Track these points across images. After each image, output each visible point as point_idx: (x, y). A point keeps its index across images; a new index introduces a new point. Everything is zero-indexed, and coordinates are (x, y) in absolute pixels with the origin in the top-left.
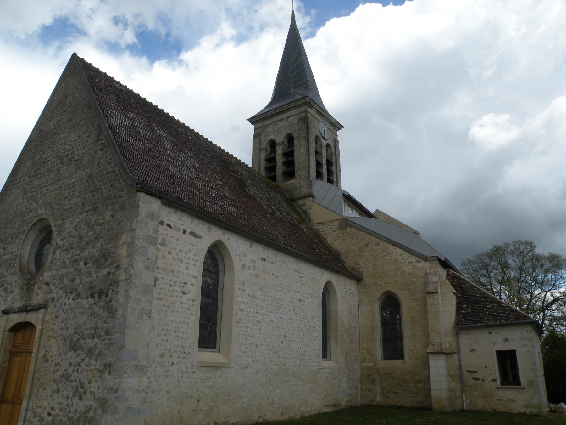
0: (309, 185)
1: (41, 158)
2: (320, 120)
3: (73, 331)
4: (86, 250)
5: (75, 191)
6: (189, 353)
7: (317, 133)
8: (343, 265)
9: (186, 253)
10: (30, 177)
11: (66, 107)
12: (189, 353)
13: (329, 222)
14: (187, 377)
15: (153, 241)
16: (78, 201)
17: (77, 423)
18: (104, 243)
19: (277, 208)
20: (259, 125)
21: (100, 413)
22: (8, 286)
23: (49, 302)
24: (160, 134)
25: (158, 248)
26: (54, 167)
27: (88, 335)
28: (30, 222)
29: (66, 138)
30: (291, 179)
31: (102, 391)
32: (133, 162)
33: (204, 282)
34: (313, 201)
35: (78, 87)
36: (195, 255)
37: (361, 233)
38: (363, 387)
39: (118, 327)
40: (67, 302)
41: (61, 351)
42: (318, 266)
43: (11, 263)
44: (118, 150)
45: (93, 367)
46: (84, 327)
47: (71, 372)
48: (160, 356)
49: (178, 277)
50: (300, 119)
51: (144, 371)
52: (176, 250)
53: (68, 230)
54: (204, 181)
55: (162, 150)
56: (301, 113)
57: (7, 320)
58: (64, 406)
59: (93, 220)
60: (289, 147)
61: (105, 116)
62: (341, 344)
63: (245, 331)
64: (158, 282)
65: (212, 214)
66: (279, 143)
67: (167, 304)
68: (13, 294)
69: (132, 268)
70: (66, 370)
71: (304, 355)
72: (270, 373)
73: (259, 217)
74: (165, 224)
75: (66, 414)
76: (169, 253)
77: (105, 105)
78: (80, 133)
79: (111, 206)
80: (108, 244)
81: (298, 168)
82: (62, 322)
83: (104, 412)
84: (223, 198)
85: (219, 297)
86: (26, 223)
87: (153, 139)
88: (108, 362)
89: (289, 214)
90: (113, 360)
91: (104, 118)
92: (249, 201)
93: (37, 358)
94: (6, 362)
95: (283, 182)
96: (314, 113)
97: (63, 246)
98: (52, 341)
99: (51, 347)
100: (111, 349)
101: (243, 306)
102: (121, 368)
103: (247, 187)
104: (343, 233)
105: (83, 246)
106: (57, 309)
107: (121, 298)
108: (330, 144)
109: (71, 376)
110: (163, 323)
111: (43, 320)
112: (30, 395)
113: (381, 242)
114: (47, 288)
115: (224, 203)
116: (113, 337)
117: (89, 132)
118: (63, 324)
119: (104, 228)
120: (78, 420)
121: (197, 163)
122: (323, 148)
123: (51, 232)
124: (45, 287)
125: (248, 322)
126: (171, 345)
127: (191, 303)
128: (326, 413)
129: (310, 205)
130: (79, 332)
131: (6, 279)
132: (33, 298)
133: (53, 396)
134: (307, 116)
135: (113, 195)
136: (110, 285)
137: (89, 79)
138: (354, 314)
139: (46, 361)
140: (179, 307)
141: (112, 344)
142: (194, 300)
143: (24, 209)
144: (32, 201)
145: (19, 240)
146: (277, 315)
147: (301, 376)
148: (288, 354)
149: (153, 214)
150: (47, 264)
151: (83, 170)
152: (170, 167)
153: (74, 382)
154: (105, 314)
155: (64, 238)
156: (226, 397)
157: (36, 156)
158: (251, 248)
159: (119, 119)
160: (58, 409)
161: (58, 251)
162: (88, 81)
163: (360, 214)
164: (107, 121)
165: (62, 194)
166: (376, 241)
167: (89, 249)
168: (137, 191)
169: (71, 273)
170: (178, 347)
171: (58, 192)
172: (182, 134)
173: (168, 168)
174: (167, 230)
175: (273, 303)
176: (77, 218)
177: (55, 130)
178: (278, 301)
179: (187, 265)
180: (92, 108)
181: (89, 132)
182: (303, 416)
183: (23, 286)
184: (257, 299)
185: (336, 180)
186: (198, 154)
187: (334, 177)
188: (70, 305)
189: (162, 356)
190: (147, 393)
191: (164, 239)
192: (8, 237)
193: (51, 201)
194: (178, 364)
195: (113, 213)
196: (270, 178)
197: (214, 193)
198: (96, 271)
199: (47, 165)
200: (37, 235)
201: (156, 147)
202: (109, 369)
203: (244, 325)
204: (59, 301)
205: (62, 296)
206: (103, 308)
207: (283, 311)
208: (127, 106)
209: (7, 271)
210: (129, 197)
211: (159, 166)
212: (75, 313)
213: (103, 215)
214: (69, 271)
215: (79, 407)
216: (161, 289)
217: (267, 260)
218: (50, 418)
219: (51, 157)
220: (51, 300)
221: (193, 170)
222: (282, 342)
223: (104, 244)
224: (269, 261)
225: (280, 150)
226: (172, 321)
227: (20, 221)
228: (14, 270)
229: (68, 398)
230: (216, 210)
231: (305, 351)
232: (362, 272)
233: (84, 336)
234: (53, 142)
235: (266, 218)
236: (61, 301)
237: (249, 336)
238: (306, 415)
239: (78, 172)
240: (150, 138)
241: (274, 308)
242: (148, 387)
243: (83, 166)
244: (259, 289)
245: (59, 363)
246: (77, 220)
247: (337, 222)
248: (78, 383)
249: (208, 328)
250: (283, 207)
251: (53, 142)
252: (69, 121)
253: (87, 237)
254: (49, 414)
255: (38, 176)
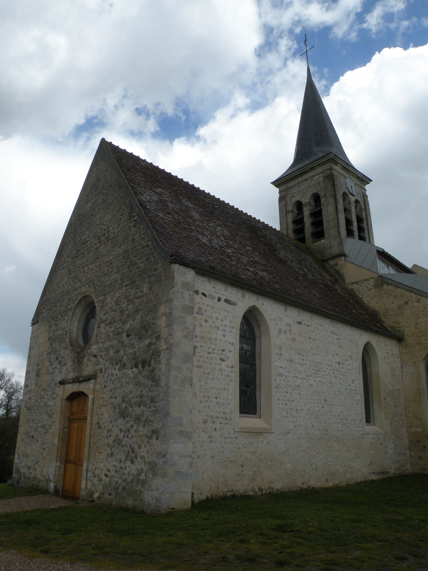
0: (340, 244)
1: (81, 239)
2: (346, 176)
3: (121, 399)
4: (127, 323)
5: (113, 267)
6: (230, 419)
7: (344, 190)
8: (383, 325)
9: (222, 320)
10: (72, 258)
11: (99, 190)
12: (230, 419)
13: (364, 281)
14: (230, 443)
15: (189, 310)
16: (117, 277)
17: (131, 484)
18: (144, 315)
19: (309, 270)
20: (284, 187)
21: (151, 476)
22: (61, 359)
23: (98, 373)
24: (187, 205)
25: (195, 317)
26: (93, 247)
27: (135, 403)
28: (76, 300)
29: (102, 219)
30: (320, 239)
31: (151, 456)
32: (165, 235)
33: (241, 349)
34: (345, 260)
35: (109, 169)
36: (231, 322)
37: (399, 290)
38: (413, 454)
39: (162, 395)
40: (114, 372)
41: (112, 418)
42: (356, 327)
43: (62, 338)
44: (150, 225)
45: (141, 433)
46: (131, 396)
47: (122, 437)
48: (203, 422)
49: (216, 345)
50: (325, 177)
51: (188, 436)
52: (212, 318)
53: (109, 305)
54: (234, 248)
55: (191, 221)
56: (326, 170)
57: (64, 390)
58: (118, 468)
59: (132, 294)
60: (316, 206)
61: (135, 194)
62: (385, 407)
63: (285, 396)
64: (197, 350)
65: (245, 280)
66: (306, 203)
67: (207, 372)
68: (67, 366)
69: (171, 338)
70: (117, 436)
71: (346, 419)
72: (312, 438)
73: (292, 281)
74: (200, 293)
75: (120, 476)
76: (206, 321)
77: (134, 183)
78: (114, 212)
79: (148, 280)
80: (147, 316)
81: (327, 228)
82: (111, 391)
83: (154, 475)
84: (254, 263)
85: (257, 362)
86: (72, 301)
87: (182, 211)
88: (155, 428)
89: (321, 275)
90: (159, 426)
91: (134, 196)
92: (280, 265)
93: (91, 425)
94: (66, 428)
95: (313, 243)
96: (340, 169)
97: (106, 320)
98: (103, 409)
99: (102, 414)
100: (157, 416)
101: (281, 371)
102: (167, 434)
103: (277, 251)
104: (380, 291)
105: (124, 319)
106: (106, 379)
107: (163, 367)
108: (359, 200)
109: (122, 441)
110: (205, 390)
111: (94, 390)
112: (89, 458)
113: (423, 299)
114: (95, 360)
115: (256, 268)
116: (158, 404)
117: (121, 211)
118: (112, 393)
119: (143, 301)
120: (132, 481)
121: (226, 231)
122: (352, 205)
123: (95, 307)
124: (92, 358)
125: (288, 387)
126: (213, 411)
127: (230, 369)
128: (373, 481)
129: (343, 264)
130: (126, 400)
131: (60, 353)
132: (84, 370)
133: (108, 459)
134: (332, 173)
135: (149, 269)
136: (152, 355)
137: (117, 161)
138: (397, 376)
139: (100, 427)
140: (218, 374)
141: (157, 411)
142: (232, 367)
143: (70, 288)
144: (76, 280)
145: (68, 316)
146: (316, 379)
147: (344, 442)
148: (330, 419)
149: (188, 284)
150: (94, 338)
151: (119, 247)
152: (200, 237)
153: (125, 447)
154: (149, 383)
155: (107, 313)
156: (269, 463)
157: (76, 238)
158: (286, 312)
159: (148, 195)
160: (113, 471)
161: (102, 325)
162: (117, 163)
163: (397, 271)
164: (137, 198)
165: (102, 271)
166: (416, 297)
167: (130, 322)
168: (172, 263)
169: (116, 345)
170: (219, 413)
171: (98, 270)
172: (209, 204)
173: (198, 239)
174: (202, 299)
175: (311, 367)
176: (117, 293)
177: (92, 212)
178: (316, 365)
179: (223, 332)
180: (123, 188)
181: (121, 211)
182: (348, 483)
183: (75, 359)
184: (295, 363)
185: (368, 236)
186: (226, 222)
187: (366, 234)
188: (116, 375)
189: (205, 422)
190: (193, 458)
191: (200, 308)
192: (58, 315)
193: (92, 278)
194: (220, 430)
195: (149, 285)
196: (299, 240)
197: (245, 260)
198: (138, 342)
199: (87, 246)
200: (83, 311)
201: (185, 219)
202: (156, 435)
203: (283, 390)
204: (106, 372)
205: (108, 368)
206: (147, 377)
207: (322, 374)
208: (155, 182)
209: (60, 345)
210: (163, 269)
211: (190, 237)
212: (122, 383)
213: (141, 289)
214: (113, 343)
215: (131, 470)
216: (201, 356)
217: (303, 323)
218: (108, 479)
219: (89, 237)
220: (99, 371)
221: (222, 238)
222: (323, 407)
223: (144, 316)
224: (304, 324)
225: (306, 211)
226: (213, 388)
227: (67, 300)
228: (66, 344)
229: (121, 461)
230: (248, 276)
231: (347, 416)
232: (403, 331)
233: (131, 404)
234: (90, 224)
235: (299, 280)
236: (108, 371)
237: (289, 400)
238: (352, 482)
239: (115, 250)
240: (179, 211)
241: (313, 372)
242: (193, 452)
243: (119, 244)
244: (296, 353)
245: (111, 429)
246: (117, 295)
247: (372, 281)
248: (129, 447)
249: (248, 394)
250: (314, 268)
251: (90, 224)
252: (103, 203)
253: (128, 310)
254: (106, 476)
255: (80, 256)
